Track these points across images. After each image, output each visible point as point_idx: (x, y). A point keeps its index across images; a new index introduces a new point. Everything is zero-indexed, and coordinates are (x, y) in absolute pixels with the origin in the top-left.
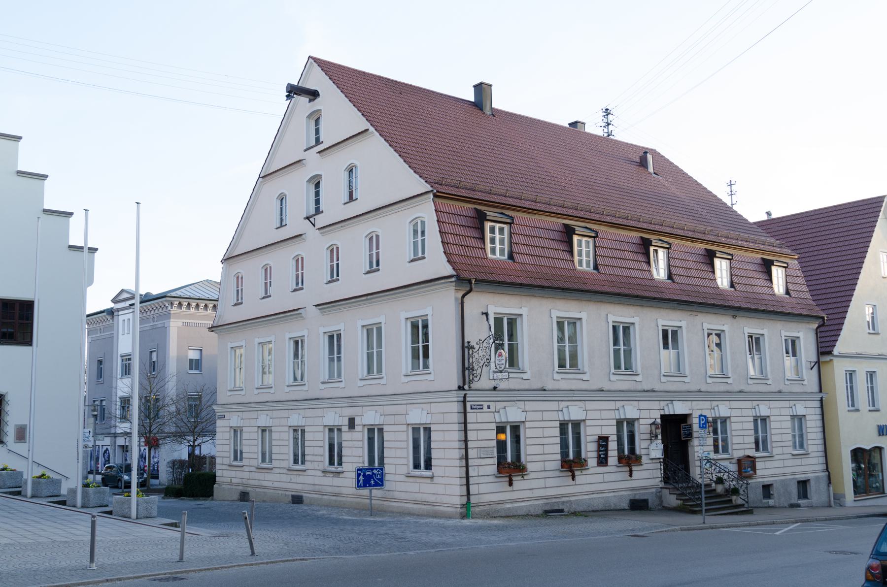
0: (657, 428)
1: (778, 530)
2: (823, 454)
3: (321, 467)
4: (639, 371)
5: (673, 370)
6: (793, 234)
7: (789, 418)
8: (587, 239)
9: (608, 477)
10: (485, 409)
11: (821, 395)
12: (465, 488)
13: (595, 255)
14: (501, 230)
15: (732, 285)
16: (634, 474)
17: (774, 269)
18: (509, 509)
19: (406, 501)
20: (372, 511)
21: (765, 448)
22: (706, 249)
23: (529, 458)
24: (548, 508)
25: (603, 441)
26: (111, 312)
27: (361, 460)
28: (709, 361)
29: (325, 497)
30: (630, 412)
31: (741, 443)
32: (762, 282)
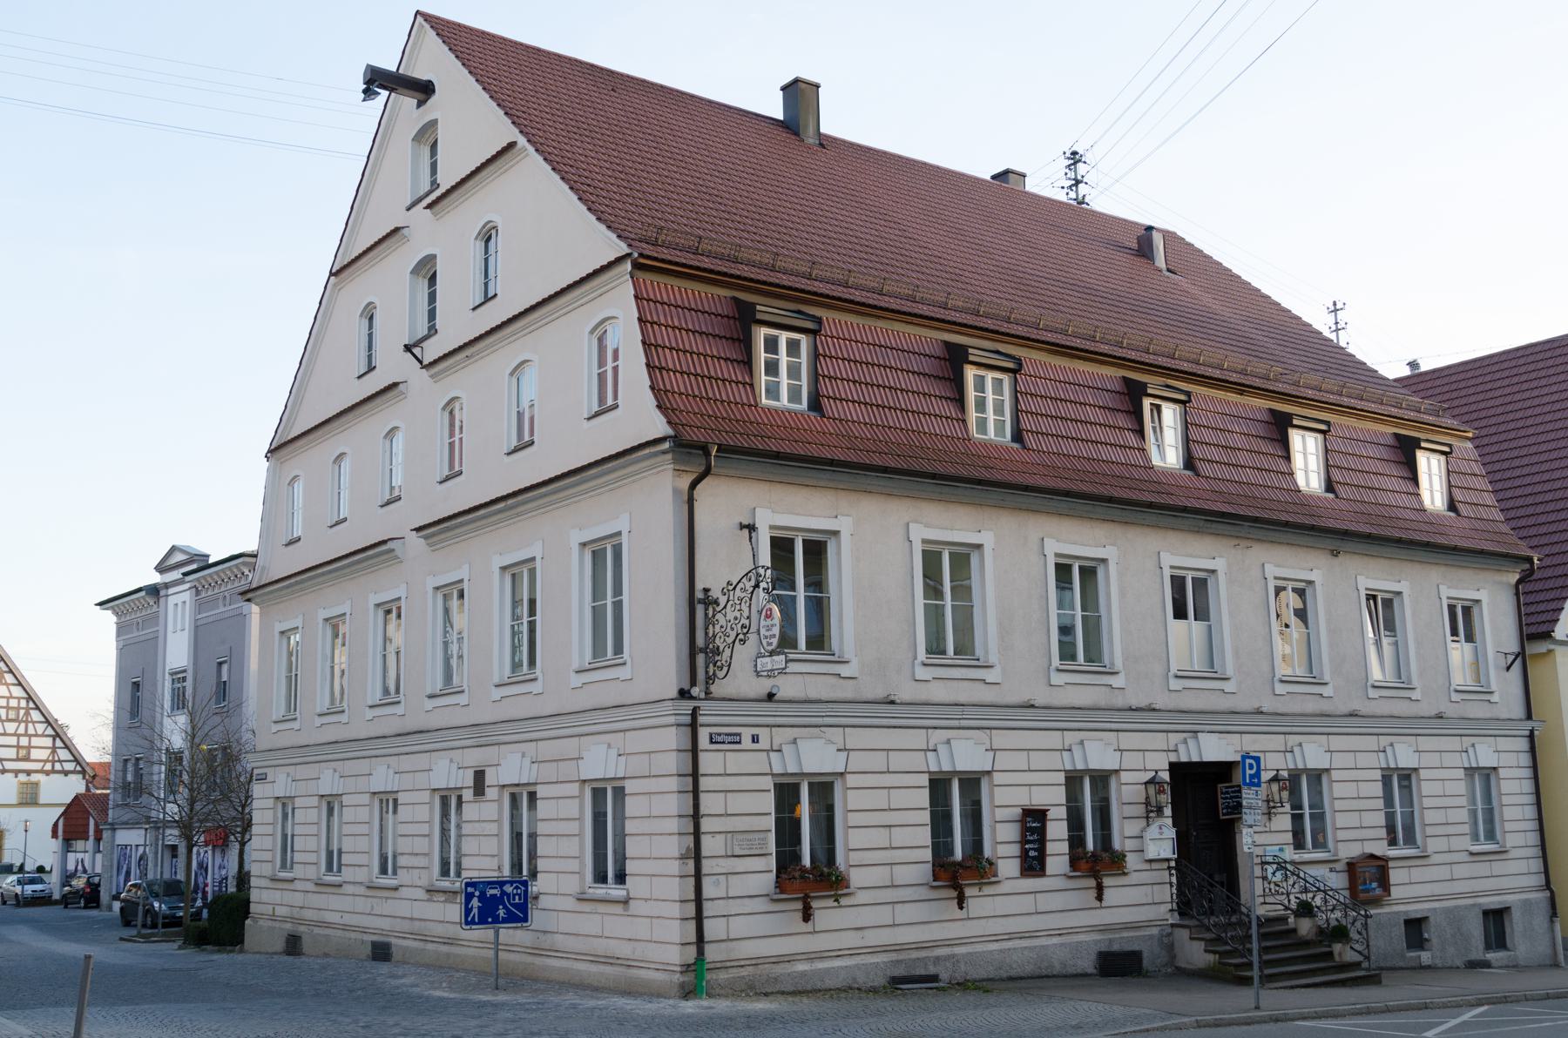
0: (1161, 792)
1: (1431, 1026)
2: (1537, 851)
3: (424, 882)
4: (1119, 665)
5: (1198, 664)
6: (1464, 401)
7: (1461, 774)
8: (998, 375)
9: (1045, 902)
10: (747, 742)
11: (1529, 725)
12: (692, 925)
13: (1016, 412)
14: (793, 347)
15: (1330, 486)
16: (1107, 893)
17: (1422, 459)
18: (803, 974)
19: (579, 956)
20: (500, 977)
21: (1410, 839)
22: (1271, 411)
23: (855, 858)
24: (900, 972)
25: (1033, 821)
26: (154, 591)
27: (494, 863)
28: (1280, 647)
29: (430, 946)
30: (1098, 754)
31: (1356, 826)
32: (1393, 481)
